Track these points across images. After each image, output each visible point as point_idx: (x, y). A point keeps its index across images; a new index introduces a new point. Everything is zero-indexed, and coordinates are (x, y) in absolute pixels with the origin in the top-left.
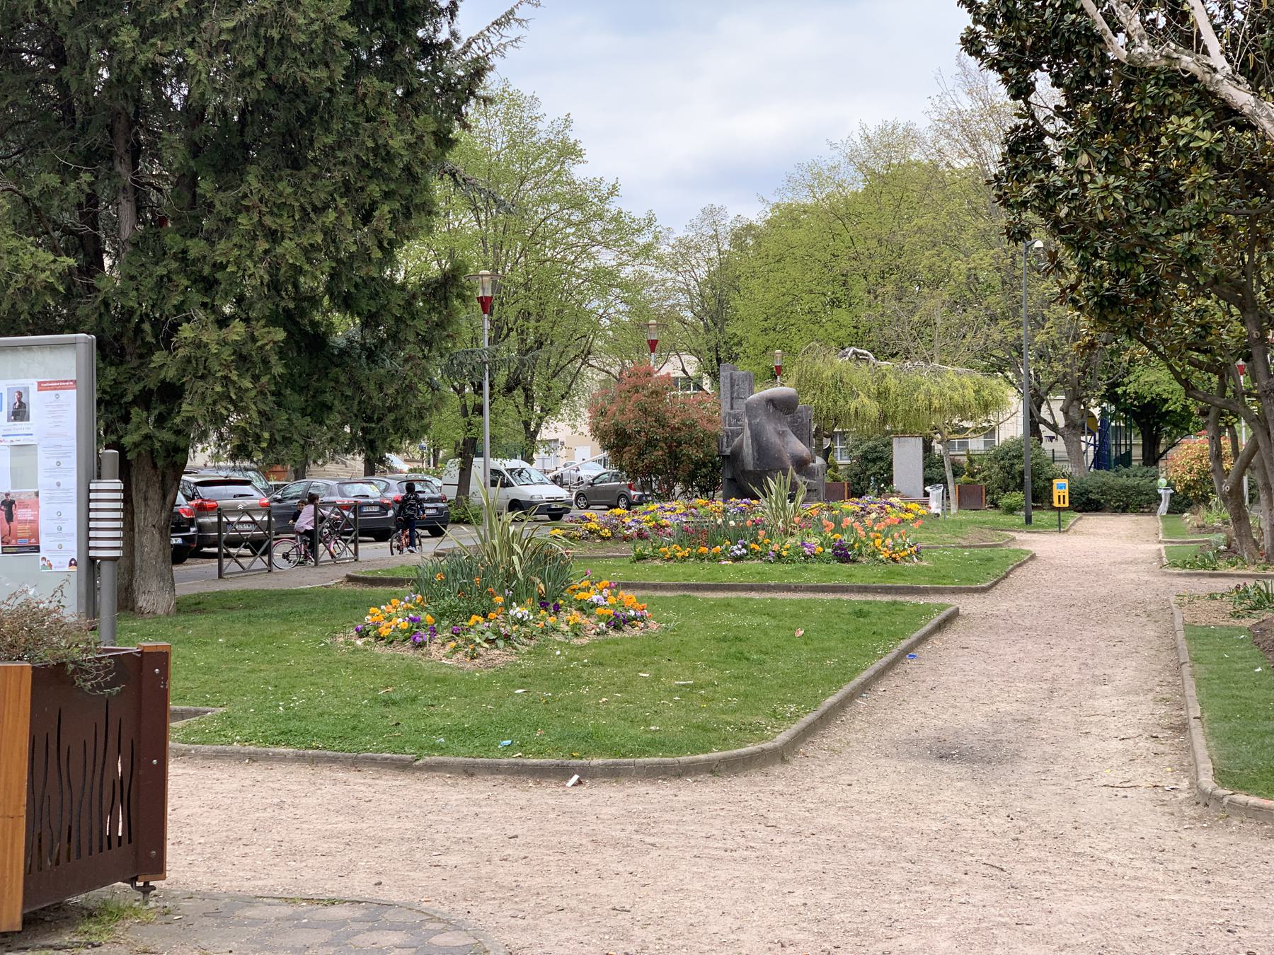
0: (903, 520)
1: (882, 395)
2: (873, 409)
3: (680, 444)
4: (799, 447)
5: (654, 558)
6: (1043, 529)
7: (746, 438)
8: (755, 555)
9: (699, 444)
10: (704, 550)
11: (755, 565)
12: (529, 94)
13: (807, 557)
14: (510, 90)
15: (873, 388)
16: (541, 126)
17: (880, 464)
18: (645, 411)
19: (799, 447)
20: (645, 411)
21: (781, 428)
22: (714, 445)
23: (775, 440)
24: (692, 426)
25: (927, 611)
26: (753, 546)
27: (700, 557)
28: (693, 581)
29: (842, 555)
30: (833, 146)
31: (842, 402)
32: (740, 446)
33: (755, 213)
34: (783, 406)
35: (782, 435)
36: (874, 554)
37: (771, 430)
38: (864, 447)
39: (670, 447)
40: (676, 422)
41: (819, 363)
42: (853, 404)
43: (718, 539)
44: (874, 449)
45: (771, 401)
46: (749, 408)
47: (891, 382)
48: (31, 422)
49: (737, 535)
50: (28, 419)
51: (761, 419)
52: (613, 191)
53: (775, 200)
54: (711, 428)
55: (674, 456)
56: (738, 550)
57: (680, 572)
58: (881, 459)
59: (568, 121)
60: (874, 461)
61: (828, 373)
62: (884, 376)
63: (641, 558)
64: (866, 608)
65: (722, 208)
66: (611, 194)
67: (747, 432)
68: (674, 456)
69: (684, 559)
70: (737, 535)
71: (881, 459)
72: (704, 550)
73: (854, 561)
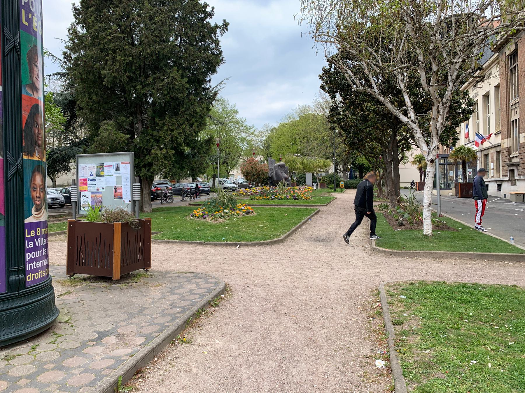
1: (303, 164)
2: (301, 167)
4: (286, 175)
5: (255, 199)
8: (276, 198)
9: (264, 175)
10: (265, 197)
15: (301, 162)
16: (229, 106)
19: (286, 175)
24: (263, 171)
25: (314, 210)
27: (265, 199)
29: (295, 198)
30: (292, 110)
33: (276, 125)
34: (282, 167)
36: (302, 198)
37: (279, 172)
38: (299, 175)
40: (259, 170)
42: (297, 166)
45: (280, 166)
47: (305, 161)
53: (280, 122)
56: (273, 197)
57: (260, 202)
60: (302, 178)
63: (252, 199)
67: (274, 172)
69: (261, 199)
71: (303, 178)
72: (265, 197)
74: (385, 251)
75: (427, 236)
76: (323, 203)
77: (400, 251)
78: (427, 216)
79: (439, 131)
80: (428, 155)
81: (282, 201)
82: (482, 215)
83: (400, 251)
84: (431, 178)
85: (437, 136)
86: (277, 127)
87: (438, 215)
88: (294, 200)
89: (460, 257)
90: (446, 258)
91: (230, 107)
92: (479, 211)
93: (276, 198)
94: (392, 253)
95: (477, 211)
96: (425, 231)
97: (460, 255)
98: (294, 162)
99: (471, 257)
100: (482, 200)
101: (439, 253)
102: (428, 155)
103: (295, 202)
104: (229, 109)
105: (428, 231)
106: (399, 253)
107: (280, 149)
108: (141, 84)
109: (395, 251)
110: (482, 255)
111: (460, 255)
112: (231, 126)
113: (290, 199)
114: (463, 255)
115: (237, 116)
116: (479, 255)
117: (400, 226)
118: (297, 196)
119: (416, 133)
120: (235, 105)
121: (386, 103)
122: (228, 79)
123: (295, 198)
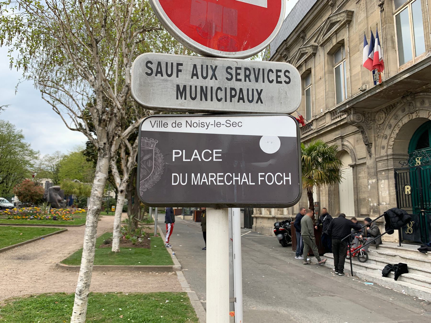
0: (79, 213)
1: (80, 189)
2: (78, 191)
3: (33, 196)
4: (60, 198)
5: (12, 219)
6: (110, 215)
7: (48, 196)
8: (36, 218)
9: (38, 196)
10: (24, 217)
11: (35, 220)
12: (13, 124)
13: (47, 219)
14: (9, 123)
15: (78, 187)
16: (15, 131)
17: (85, 202)
18: (26, 189)
19: (60, 198)
20: (26, 189)
21: (56, 194)
22: (41, 197)
23: (54, 196)
24: (37, 193)
25: (59, 229)
26: (35, 217)
27: (23, 219)
28: (17, 223)
29: (55, 219)
30: (83, 142)
31: (71, 190)
32: (47, 197)
33: (67, 153)
34: (57, 190)
35: (56, 195)
36: (62, 219)
37: (53, 194)
38: (82, 199)
39: (31, 196)
40: (33, 192)
41: (68, 182)
42: (74, 190)
43: (28, 215)
44: (84, 199)
45: (54, 188)
46: (50, 190)
47: (82, 186)
48: (115, 216)
49: (32, 214)
50: (114, 216)
51: (52, 192)
52: (29, 145)
53: (70, 151)
54: (41, 193)
55: (32, 198)
56: (32, 217)
57: (21, 221)
58: (85, 201)
59: (21, 131)
60: (84, 201)
61: (69, 184)
62: (81, 185)
63: (9, 218)
64: (44, 229)
65: (60, 152)
66: (29, 146)
67: (49, 194)
68: (32, 198)
69: (19, 219)
70: (32, 214)
71: (85, 201)
72: (24, 217)
73: (57, 220)
74: (63, 267)
75: (114, 252)
76: (78, 224)
77: (75, 266)
78: (115, 236)
79: (130, 168)
80: (120, 186)
81: (40, 221)
82: (170, 235)
83: (75, 266)
84: (120, 205)
85: (127, 172)
86: (68, 155)
87: (155, 236)
88: (53, 221)
89: (123, 269)
90: (112, 270)
91: (16, 132)
92: (168, 232)
93: (36, 218)
94: (68, 268)
95: (167, 232)
96: (113, 248)
97: (123, 268)
98: (72, 187)
99: (131, 270)
100: (171, 223)
101: (107, 267)
102: (120, 186)
103: (55, 222)
104: (16, 133)
105: (115, 248)
106: (73, 267)
107: (68, 175)
108: (116, 113)
109: (71, 266)
110: (139, 268)
111: (123, 268)
112: (18, 149)
113: (49, 219)
114: (125, 268)
115: (23, 141)
116: (137, 267)
117: (106, 244)
118: (57, 217)
119: (113, 169)
120: (21, 131)
121: (94, 143)
122: (7, 106)
123: (55, 219)
